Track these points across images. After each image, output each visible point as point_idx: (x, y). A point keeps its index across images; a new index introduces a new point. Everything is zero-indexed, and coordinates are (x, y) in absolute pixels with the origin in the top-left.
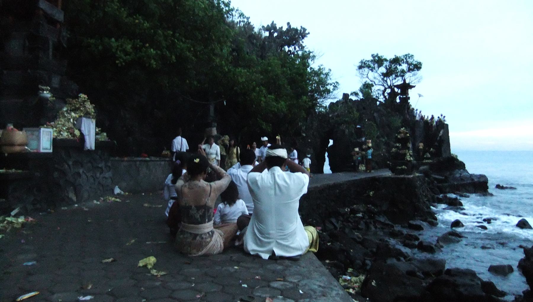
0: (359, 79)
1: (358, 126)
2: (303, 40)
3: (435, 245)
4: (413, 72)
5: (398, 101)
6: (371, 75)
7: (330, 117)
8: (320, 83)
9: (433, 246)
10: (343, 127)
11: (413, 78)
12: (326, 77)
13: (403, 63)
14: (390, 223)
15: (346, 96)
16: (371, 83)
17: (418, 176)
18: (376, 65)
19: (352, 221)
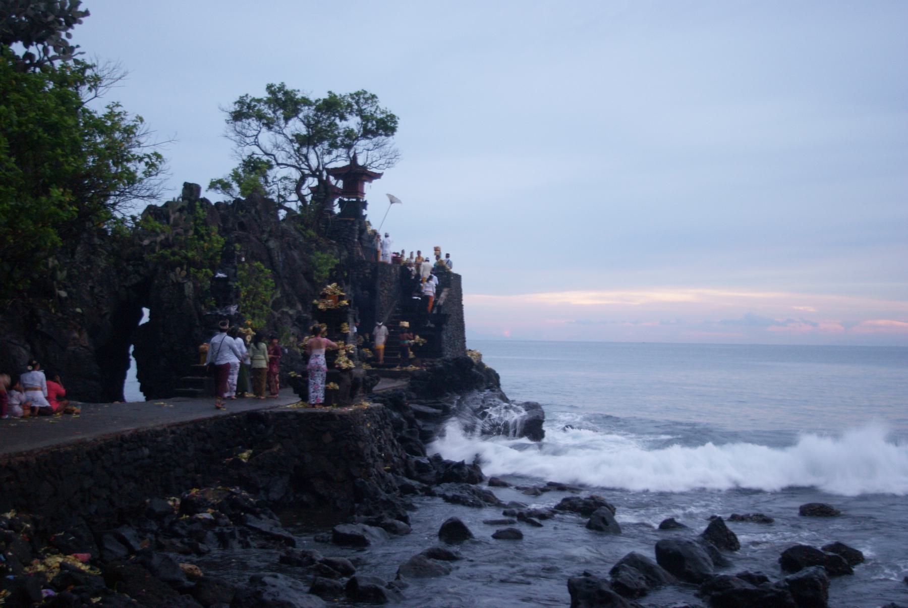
0: (234, 144)
1: (220, 275)
2: (70, 31)
3: (390, 586)
4: (375, 140)
5: (337, 210)
6: (267, 138)
7: (144, 248)
8: (111, 151)
9: (383, 588)
10: (179, 274)
11: (376, 153)
12: (128, 139)
13: (351, 113)
14: (286, 534)
15: (191, 190)
16: (265, 158)
17: (370, 409)
18: (280, 113)
19: (183, 532)
